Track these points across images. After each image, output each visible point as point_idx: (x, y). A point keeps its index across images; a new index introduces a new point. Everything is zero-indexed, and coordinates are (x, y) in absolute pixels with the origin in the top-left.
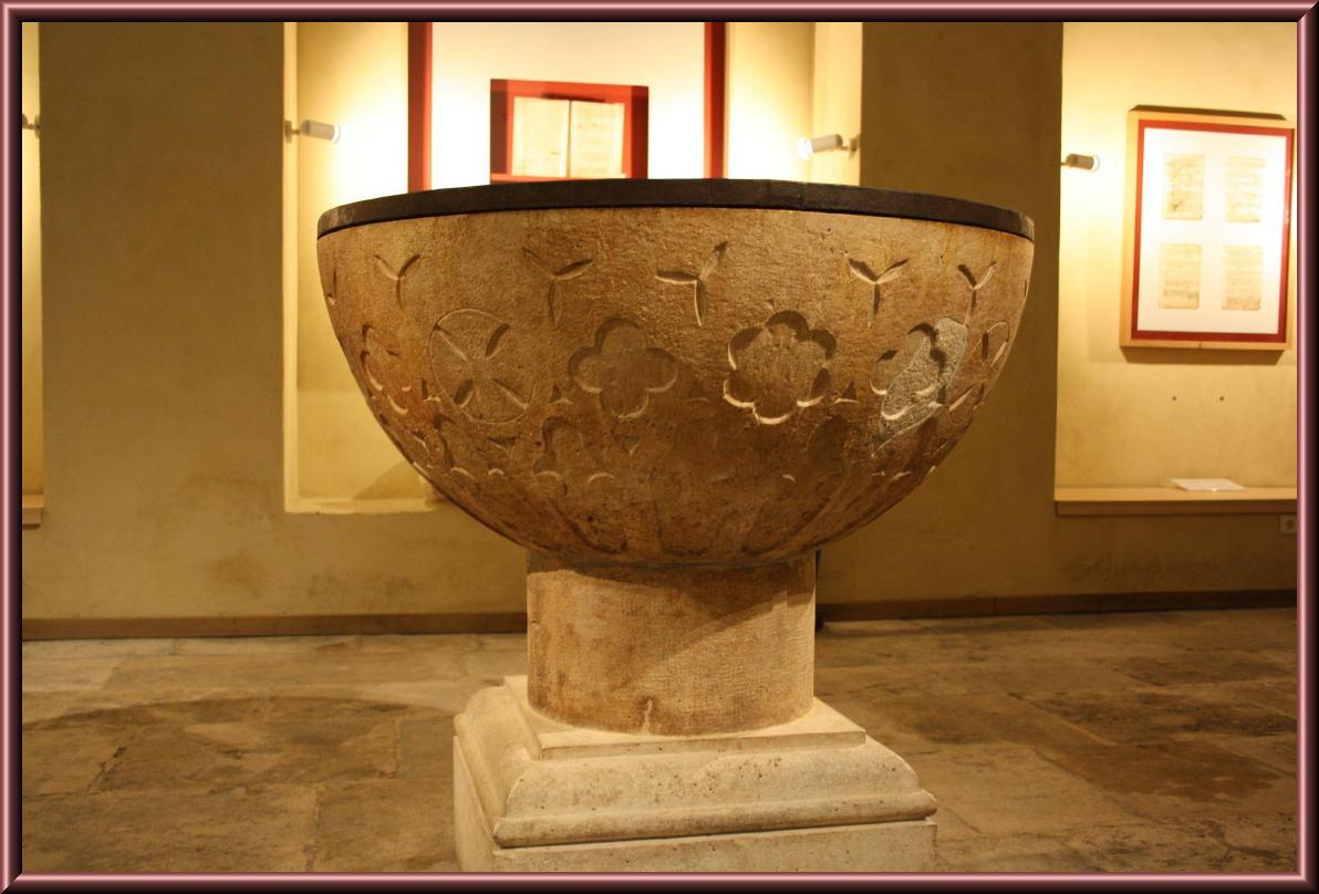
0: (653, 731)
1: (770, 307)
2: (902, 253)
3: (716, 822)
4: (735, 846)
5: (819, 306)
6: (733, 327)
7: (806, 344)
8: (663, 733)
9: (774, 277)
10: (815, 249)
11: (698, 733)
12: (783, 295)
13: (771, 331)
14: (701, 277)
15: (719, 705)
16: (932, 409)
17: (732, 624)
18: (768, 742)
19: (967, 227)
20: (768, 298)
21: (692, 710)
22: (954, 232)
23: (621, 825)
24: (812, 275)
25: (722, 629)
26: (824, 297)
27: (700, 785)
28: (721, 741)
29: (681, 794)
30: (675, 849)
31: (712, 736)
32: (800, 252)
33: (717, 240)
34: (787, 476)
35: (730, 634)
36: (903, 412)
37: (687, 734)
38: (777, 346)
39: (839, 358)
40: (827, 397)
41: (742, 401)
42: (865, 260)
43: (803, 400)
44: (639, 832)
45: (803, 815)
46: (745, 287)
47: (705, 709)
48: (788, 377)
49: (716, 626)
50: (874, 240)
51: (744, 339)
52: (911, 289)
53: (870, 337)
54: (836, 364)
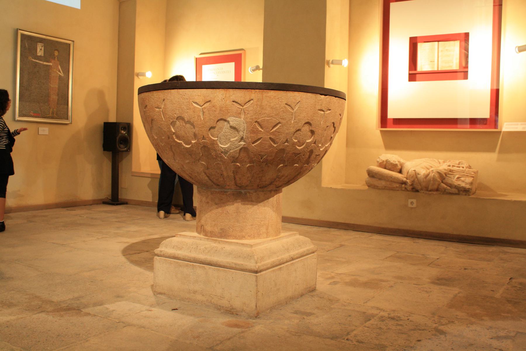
0: (203, 235)
1: (176, 115)
2: (208, 99)
3: (200, 260)
4: (205, 268)
5: (187, 115)
6: (170, 121)
7: (187, 125)
8: (205, 236)
9: (175, 107)
10: (182, 99)
11: (211, 237)
13: (179, 122)
15: (216, 230)
16: (242, 145)
17: (221, 207)
18: (226, 243)
19: (157, 91)
20: (175, 113)
21: (210, 230)
22: (228, 91)
23: (179, 256)
24: (183, 106)
25: (217, 208)
26: (187, 112)
27: (201, 250)
28: (215, 240)
29: (196, 251)
30: (191, 265)
31: (214, 239)
32: (179, 100)
33: (163, 98)
34: (238, 164)
35: (220, 210)
36: (228, 145)
37: (209, 237)
38: (181, 125)
39: (197, 129)
40: (198, 139)
41: (180, 141)
42: (196, 101)
43: (193, 141)
44: (183, 259)
45: (221, 264)
46: (169, 110)
47: (213, 230)
48: (186, 134)
49: (216, 207)
50: (198, 96)
51: (173, 124)
52: (214, 109)
53: (204, 123)
54: (196, 130)
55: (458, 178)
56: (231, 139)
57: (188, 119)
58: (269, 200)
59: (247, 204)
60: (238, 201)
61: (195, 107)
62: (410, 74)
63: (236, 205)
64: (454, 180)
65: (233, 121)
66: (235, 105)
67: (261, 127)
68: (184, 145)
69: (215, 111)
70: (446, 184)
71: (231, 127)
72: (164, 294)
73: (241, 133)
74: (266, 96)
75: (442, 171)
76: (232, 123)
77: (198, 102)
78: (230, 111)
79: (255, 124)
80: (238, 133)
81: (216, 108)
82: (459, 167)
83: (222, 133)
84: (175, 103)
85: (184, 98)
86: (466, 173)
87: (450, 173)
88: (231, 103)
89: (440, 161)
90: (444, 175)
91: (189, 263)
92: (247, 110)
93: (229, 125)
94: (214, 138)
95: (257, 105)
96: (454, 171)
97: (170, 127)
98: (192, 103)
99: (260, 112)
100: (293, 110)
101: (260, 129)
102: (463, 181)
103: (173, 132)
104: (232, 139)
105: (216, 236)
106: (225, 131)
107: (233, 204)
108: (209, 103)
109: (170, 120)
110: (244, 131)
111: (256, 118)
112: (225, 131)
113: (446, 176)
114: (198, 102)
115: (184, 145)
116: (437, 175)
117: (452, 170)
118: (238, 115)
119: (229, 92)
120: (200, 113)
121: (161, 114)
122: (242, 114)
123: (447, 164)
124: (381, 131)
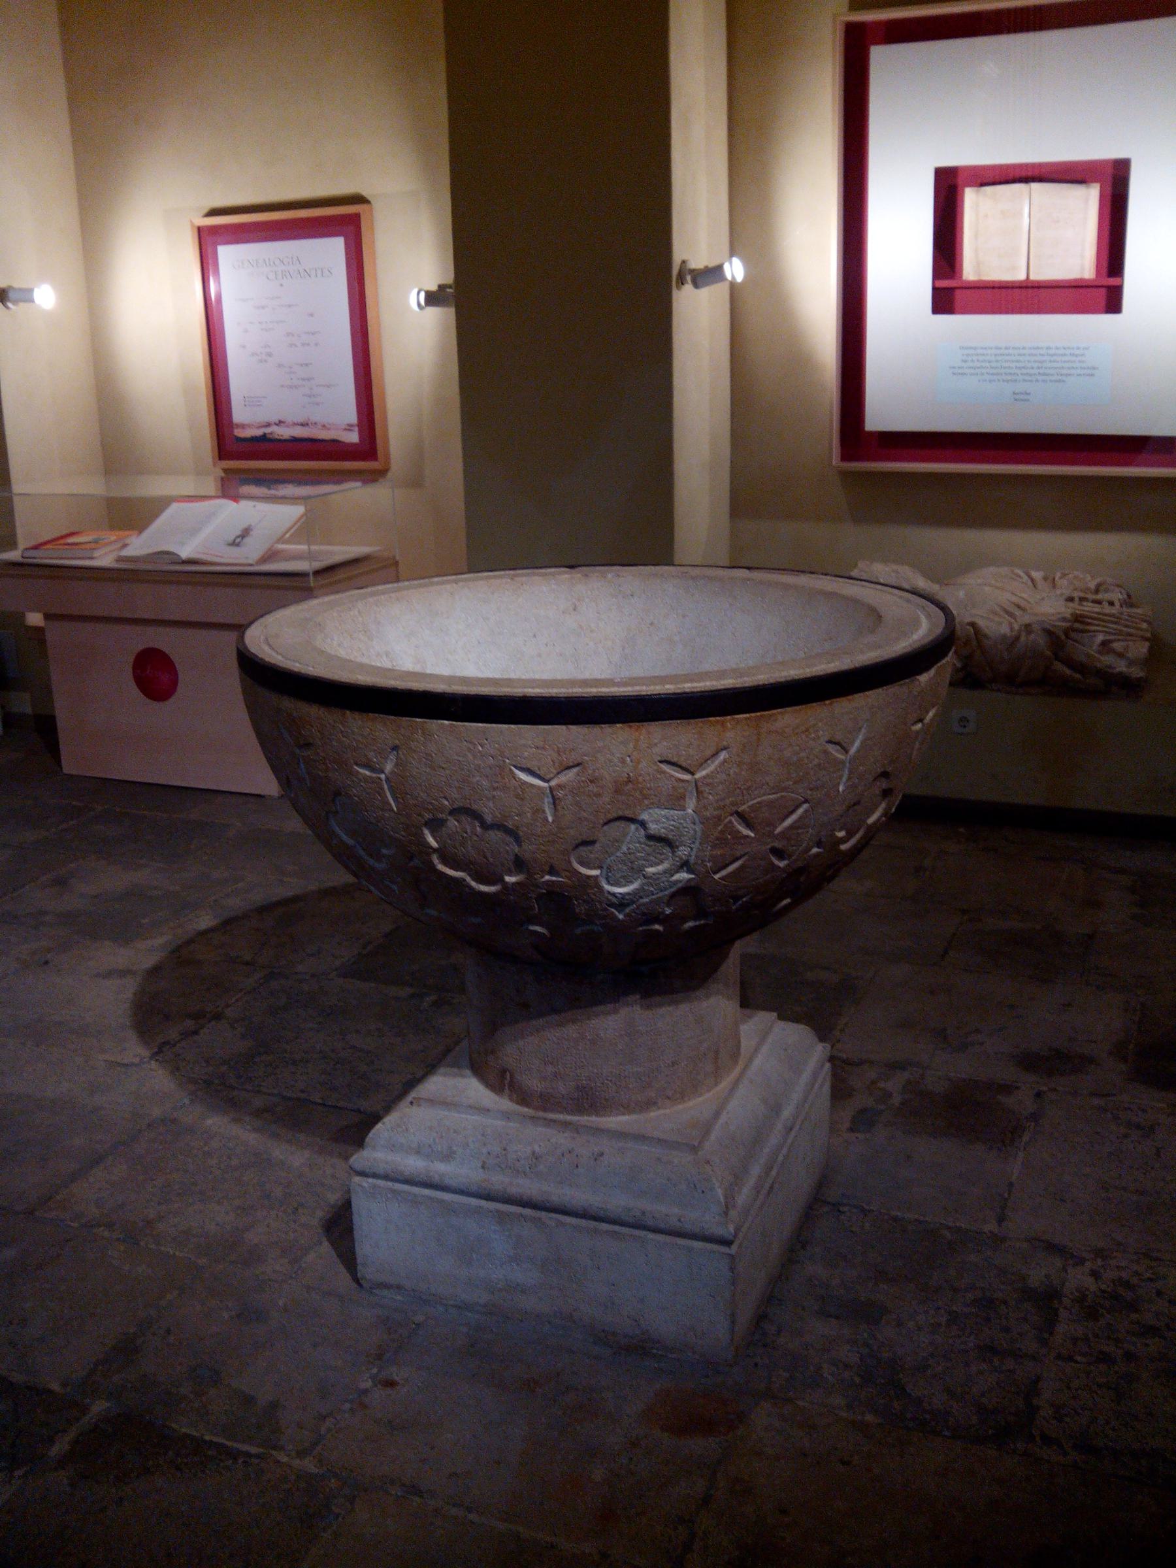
2: (574, 757)
8: (517, 1103)
10: (474, 756)
12: (455, 795)
14: (386, 771)
22: (644, 731)
23: (448, 1181)
35: (571, 1031)
41: (457, 871)
48: (485, 857)
52: (593, 788)
55: (1104, 644)
56: (646, 869)
57: (497, 817)
58: (719, 974)
59: (661, 1005)
60: (631, 998)
61: (525, 783)
62: (935, 289)
63: (624, 1012)
64: (1089, 648)
65: (658, 819)
66: (668, 770)
67: (749, 825)
68: (473, 884)
69: (598, 795)
70: (1070, 663)
71: (650, 837)
72: (399, 1287)
73: (683, 852)
74: (769, 732)
75: (1057, 623)
76: (653, 828)
77: (536, 769)
78: (652, 792)
79: (730, 822)
80: (673, 852)
81: (602, 787)
82: (1099, 602)
83: (618, 854)
84: (444, 766)
85: (480, 752)
86: (1126, 626)
87: (1077, 625)
88: (655, 768)
89: (1034, 574)
90: (1063, 637)
91: (483, 1203)
92: (708, 785)
93: (642, 832)
94: (591, 868)
95: (740, 764)
96: (1089, 621)
97: (423, 834)
98: (511, 770)
99: (749, 784)
100: (846, 751)
101: (746, 832)
102: (1121, 655)
103: (431, 847)
104: (651, 870)
105: (559, 1107)
106: (629, 849)
107: (616, 1011)
108: (575, 770)
109: (423, 812)
110: (694, 843)
111: (733, 804)
112: (629, 849)
113: (1067, 636)
114: (537, 769)
115: (473, 884)
116: (1041, 641)
117: (1082, 616)
118: (676, 800)
119: (649, 733)
120: (543, 803)
121: (382, 789)
122: (688, 795)
123: (1062, 595)
124: (845, 475)
